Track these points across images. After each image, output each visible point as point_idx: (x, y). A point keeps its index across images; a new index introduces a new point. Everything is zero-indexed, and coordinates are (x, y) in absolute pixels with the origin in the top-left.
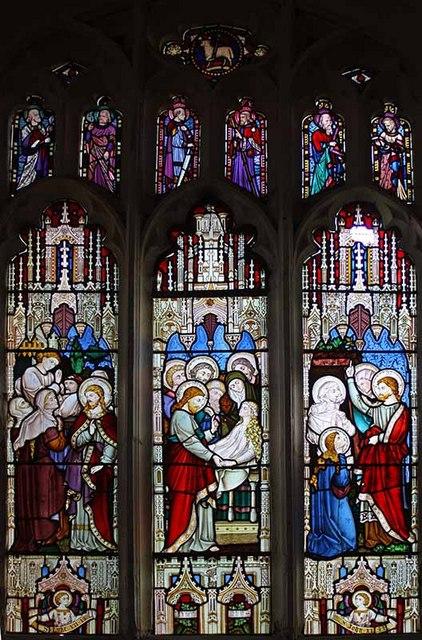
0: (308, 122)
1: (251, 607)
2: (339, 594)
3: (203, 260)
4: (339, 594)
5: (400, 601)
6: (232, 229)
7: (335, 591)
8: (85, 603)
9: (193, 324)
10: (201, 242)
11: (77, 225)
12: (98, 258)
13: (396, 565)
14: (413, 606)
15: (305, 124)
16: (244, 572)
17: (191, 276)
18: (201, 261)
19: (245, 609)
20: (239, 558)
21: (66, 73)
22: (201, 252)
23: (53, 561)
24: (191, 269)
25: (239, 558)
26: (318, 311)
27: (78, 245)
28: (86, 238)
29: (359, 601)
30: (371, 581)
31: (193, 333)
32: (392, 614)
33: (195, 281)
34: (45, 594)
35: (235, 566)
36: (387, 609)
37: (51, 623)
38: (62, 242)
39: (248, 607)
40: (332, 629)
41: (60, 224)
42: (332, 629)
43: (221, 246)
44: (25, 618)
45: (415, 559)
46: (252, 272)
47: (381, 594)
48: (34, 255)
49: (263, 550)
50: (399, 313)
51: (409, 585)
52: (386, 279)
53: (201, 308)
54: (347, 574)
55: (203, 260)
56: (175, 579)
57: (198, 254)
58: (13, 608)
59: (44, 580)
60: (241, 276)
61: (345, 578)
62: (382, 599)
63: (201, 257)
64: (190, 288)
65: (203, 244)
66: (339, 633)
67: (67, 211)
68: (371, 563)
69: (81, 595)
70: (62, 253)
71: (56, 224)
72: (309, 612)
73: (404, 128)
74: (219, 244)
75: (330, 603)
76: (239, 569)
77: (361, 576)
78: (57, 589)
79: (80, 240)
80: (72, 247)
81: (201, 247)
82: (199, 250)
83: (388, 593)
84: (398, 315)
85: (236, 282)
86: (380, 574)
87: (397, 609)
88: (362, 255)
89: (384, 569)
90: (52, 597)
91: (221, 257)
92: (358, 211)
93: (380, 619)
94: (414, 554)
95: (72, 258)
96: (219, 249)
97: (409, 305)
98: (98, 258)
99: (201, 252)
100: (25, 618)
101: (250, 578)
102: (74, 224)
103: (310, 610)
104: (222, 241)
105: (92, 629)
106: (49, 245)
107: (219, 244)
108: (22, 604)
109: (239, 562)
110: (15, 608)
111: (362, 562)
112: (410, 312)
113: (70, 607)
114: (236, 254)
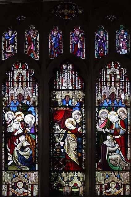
0: (5, 34)
1: (79, 187)
2: (13, 183)
3: (65, 78)
4: (13, 183)
5: (124, 185)
6: (73, 69)
7: (12, 182)
8: (27, 186)
9: (62, 98)
10: (64, 73)
11: (117, 68)
12: (123, 78)
13: (31, 174)
14: (128, 187)
15: (4, 34)
16: (77, 176)
17: (61, 84)
18: (64, 79)
19: (77, 188)
20: (76, 172)
21: (109, 18)
22: (64, 76)
23: (109, 173)
24: (61, 81)
25: (76, 172)
26: (7, 95)
27: (117, 74)
28: (120, 72)
29: (20, 185)
30: (23, 179)
31: (61, 102)
32: (30, 189)
33: (62, 85)
34: (107, 184)
35: (74, 174)
36: (28, 188)
37: (110, 192)
38: (19, 74)
39: (78, 188)
40: (11, 194)
41: (19, 68)
42: (11, 194)
43: (70, 74)
44: (8, 191)
45: (37, 172)
46: (80, 83)
47: (26, 183)
48: (104, 77)
49: (36, 170)
50: (32, 96)
51: (35, 181)
52: (121, 85)
53: (65, 94)
54: (16, 177)
55: (65, 78)
56: (72, 178)
57: (63, 77)
58: (4, 187)
59: (14, 179)
60: (77, 85)
61: (15, 178)
62: (119, 185)
63: (64, 77)
64: (61, 88)
65: (65, 74)
66: (13, 196)
67: (113, 64)
68: (23, 174)
69: (118, 183)
70: (19, 78)
71: (17, 68)
72: (4, 188)
73: (15, 34)
74: (70, 74)
75: (10, 186)
76: (75, 175)
77: (113, 177)
78: (111, 182)
79: (118, 73)
80: (23, 76)
81: (64, 74)
82: (63, 75)
83: (121, 183)
84: (32, 96)
85: (75, 86)
86: (119, 177)
87: (31, 188)
88: (21, 77)
89: (27, 175)
90: (110, 185)
91: (70, 77)
92: (20, 63)
93: (26, 191)
94: (37, 171)
95: (115, 79)
96: (70, 75)
97: (128, 93)
98: (123, 78)
99: (64, 76)
100: (8, 191)
101: (79, 178)
102: (23, 68)
103: (97, 187)
104: (70, 73)
105: (122, 194)
106: (15, 75)
107: (70, 74)
108: (100, 186)
109: (76, 173)
110: (98, 188)
111: (113, 173)
112: (128, 95)
113: (115, 188)
114: (75, 76)
